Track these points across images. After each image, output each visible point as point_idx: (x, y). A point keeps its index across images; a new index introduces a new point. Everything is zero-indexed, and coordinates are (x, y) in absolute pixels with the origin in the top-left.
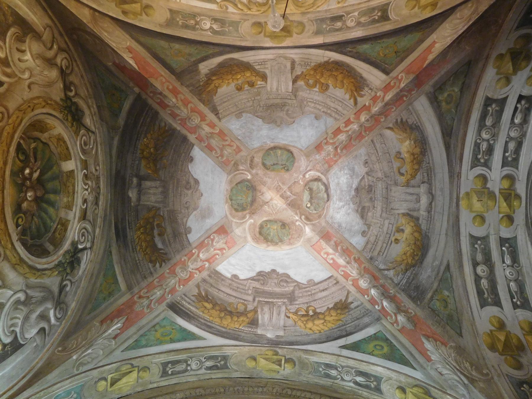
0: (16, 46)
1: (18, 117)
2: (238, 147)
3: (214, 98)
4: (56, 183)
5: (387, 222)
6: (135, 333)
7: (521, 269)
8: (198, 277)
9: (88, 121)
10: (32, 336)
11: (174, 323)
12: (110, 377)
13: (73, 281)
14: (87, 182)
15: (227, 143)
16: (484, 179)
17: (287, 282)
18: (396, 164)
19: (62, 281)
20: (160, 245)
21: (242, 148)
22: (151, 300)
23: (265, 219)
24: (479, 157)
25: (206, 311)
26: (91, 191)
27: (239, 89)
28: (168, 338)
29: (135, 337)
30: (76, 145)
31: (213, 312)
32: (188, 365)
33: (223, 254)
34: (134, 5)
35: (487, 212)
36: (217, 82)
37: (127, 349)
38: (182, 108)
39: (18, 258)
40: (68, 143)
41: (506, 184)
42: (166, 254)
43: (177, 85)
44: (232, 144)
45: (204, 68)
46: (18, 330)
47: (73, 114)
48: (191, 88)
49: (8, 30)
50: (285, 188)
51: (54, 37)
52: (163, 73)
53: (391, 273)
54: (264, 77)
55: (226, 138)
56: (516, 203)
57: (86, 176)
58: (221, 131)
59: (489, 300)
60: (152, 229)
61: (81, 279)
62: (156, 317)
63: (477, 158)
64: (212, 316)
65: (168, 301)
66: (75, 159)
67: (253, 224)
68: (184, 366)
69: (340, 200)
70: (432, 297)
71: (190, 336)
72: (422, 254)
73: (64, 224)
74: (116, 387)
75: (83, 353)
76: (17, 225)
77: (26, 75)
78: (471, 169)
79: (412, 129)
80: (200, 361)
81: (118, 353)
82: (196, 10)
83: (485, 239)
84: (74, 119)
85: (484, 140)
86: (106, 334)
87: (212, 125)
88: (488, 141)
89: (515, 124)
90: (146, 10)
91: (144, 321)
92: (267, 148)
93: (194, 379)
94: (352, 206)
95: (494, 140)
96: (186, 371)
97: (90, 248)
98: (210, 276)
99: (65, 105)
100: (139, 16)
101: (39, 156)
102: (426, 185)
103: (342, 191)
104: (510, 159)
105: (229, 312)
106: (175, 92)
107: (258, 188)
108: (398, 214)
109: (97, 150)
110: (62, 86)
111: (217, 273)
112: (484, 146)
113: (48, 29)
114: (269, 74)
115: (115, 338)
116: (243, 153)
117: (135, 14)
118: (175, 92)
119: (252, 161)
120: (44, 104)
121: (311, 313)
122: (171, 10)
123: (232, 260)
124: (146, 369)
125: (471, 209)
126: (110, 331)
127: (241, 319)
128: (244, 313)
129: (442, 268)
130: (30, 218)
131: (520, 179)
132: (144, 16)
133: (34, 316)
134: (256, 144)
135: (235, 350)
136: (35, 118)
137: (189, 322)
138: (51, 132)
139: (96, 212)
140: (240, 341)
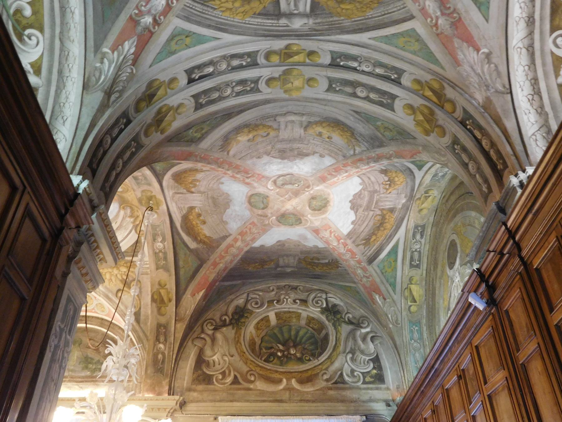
0: (212, 367)
2: (250, 224)
5: (312, 141)
7: (365, 58)
8: (351, 246)
9: (241, 301)
11: (383, 261)
12: (410, 304)
13: (346, 312)
15: (248, 231)
16: (269, 81)
17: (360, 195)
18: (259, 139)
19: (345, 322)
20: (327, 261)
21: (251, 221)
22: (364, 276)
23: (308, 208)
27: (204, 222)
28: (393, 264)
29: (388, 286)
31: (379, 235)
32: (416, 251)
34: (162, 294)
35: (304, 75)
36: (202, 237)
38: (226, 259)
41: (275, 59)
43: (210, 263)
44: (248, 227)
45: (193, 245)
46: (368, 358)
47: (240, 316)
51: (197, 338)
53: (358, 150)
55: (244, 231)
56: (295, 48)
57: (278, 301)
58: (240, 234)
60: (315, 263)
61: (346, 303)
62: (376, 272)
63: (250, 90)
64: (382, 236)
65: (366, 265)
67: (312, 215)
71: (395, 250)
72: (343, 125)
73: (310, 320)
75: (389, 320)
76: (309, 360)
77: (226, 358)
79: (226, 140)
80: (415, 242)
81: (395, 297)
82: (151, 253)
84: (242, 316)
85: (233, 91)
86: (381, 305)
87: (236, 240)
89: (214, 70)
91: (378, 280)
92: (249, 206)
95: (232, 83)
96: (420, 252)
101: (269, 345)
103: (284, 167)
104: (249, 60)
105: (380, 225)
106: (215, 264)
108: (305, 134)
110: (225, 329)
112: (238, 88)
113: (195, 343)
115: (385, 299)
116: (256, 221)
117: (168, 293)
118: (215, 264)
119: (261, 216)
120: (239, 344)
121: (389, 182)
122: (157, 269)
123: (340, 225)
124: (411, 279)
125: (300, 88)
126: (380, 302)
127: (387, 217)
128: (383, 217)
129: (357, 116)
130: (306, 351)
131: (269, 46)
133: (362, 346)
134: (247, 213)
135: (412, 220)
136: (247, 346)
137: (383, 250)
138: (254, 335)
139: (301, 288)
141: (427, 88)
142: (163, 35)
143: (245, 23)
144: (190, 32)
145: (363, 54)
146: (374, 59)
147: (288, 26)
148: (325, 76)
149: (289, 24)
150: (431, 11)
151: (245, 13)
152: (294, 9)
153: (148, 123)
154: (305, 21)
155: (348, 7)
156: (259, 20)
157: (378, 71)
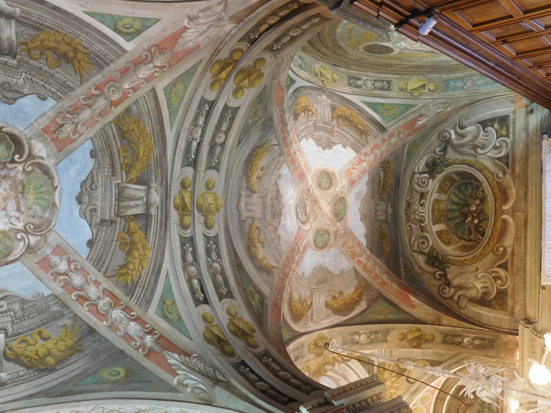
1: (486, 251)
3: (357, 284)
4: (450, 215)
5: (265, 187)
6: (408, 115)
7: (188, 135)
8: (367, 149)
9: (421, 259)
10: (470, 127)
11: (383, 117)
14: (421, 218)
15: (350, 250)
18: (262, 236)
19: (444, 155)
20: (382, 173)
21: (341, 247)
22: (398, 136)
23: (329, 191)
24: (214, 246)
25: (361, 122)
26: (416, 212)
27: (341, 293)
28: (386, 107)
30: (433, 241)
31: (357, 121)
33: (353, 165)
34: (412, 337)
36: (356, 295)
37: (414, 106)
39: (484, 173)
40: (439, 241)
41: (187, 220)
42: (381, 167)
43: (382, 289)
45: (363, 305)
46: (482, 132)
48: (372, 288)
49: (495, 297)
50: (320, 216)
51: (458, 304)
52: (391, 295)
53: (274, 142)
54: (327, 305)
55: (350, 253)
56: (178, 201)
59: (229, 112)
60: (383, 186)
61: (425, 154)
62: (394, 124)
63: (216, 245)
64: (358, 118)
65: (387, 134)
66: (432, 232)
67: (336, 187)
68: (376, 85)
69: (290, 206)
70: (260, 119)
71: (372, 105)
73: (441, 190)
74: (423, 83)
75: (443, 111)
76: (483, 191)
77: (480, 275)
78: (218, 234)
79: (262, 269)
80: (365, 86)
81: (420, 105)
82: (369, 347)
83: (209, 167)
87: (359, 262)
88: (213, 261)
90: (404, 336)
91: (402, 122)
92: (326, 248)
93: (369, 73)
94: (283, 201)
95: (209, 262)
96: (375, 81)
97: (415, 173)
98: (360, 149)
99: (445, 265)
100: (408, 330)
101: (467, 231)
102: (243, 219)
103: (289, 213)
104: (188, 245)
105: (347, 119)
106: (383, 283)
107: (333, 216)
109: (410, 240)
110: (449, 276)
111: (356, 151)
112: (214, 256)
114: (324, 308)
115: (421, 115)
116: (341, 242)
117: (411, 331)
119: (336, 237)
120: (465, 262)
122: (387, 341)
124: (402, 90)
125: (215, 196)
127: (340, 113)
128: (340, 117)
130: (473, 195)
131: (176, 225)
132: (405, 332)
133: (469, 138)
134: (333, 250)
135: (343, 89)
136: (467, 254)
139: (408, 198)
140: (340, 96)
141: (219, 76)
142: (163, 325)
143: (154, 247)
144: (160, 300)
145: (185, 136)
146: (190, 125)
147: (158, 207)
148: (205, 173)
149: (156, 206)
150: (149, 73)
151: (145, 247)
152: (142, 201)
153: (220, 353)
154: (153, 191)
155: (142, 151)
156: (152, 233)
157: (201, 122)
